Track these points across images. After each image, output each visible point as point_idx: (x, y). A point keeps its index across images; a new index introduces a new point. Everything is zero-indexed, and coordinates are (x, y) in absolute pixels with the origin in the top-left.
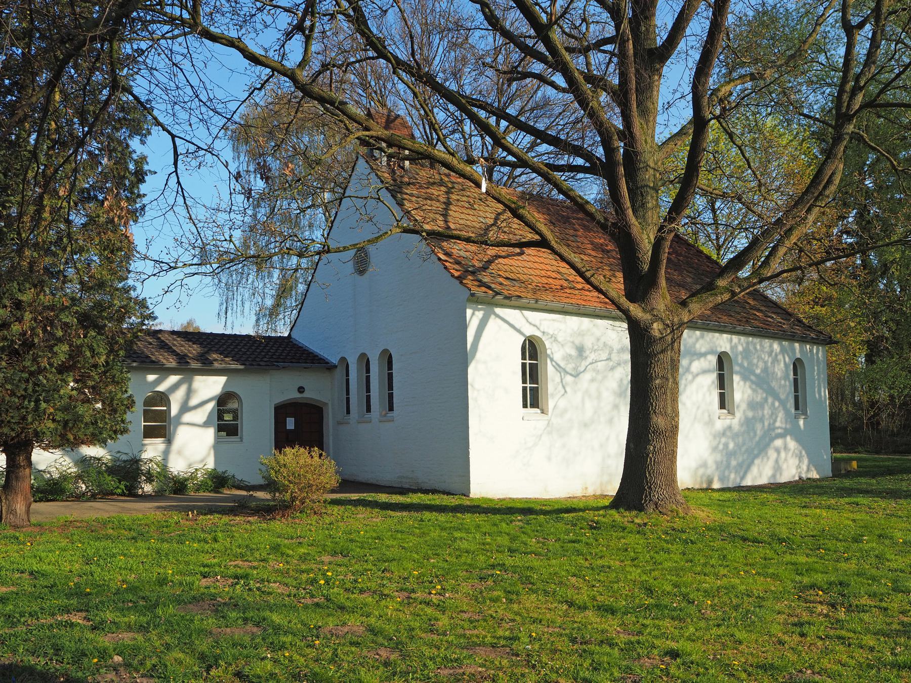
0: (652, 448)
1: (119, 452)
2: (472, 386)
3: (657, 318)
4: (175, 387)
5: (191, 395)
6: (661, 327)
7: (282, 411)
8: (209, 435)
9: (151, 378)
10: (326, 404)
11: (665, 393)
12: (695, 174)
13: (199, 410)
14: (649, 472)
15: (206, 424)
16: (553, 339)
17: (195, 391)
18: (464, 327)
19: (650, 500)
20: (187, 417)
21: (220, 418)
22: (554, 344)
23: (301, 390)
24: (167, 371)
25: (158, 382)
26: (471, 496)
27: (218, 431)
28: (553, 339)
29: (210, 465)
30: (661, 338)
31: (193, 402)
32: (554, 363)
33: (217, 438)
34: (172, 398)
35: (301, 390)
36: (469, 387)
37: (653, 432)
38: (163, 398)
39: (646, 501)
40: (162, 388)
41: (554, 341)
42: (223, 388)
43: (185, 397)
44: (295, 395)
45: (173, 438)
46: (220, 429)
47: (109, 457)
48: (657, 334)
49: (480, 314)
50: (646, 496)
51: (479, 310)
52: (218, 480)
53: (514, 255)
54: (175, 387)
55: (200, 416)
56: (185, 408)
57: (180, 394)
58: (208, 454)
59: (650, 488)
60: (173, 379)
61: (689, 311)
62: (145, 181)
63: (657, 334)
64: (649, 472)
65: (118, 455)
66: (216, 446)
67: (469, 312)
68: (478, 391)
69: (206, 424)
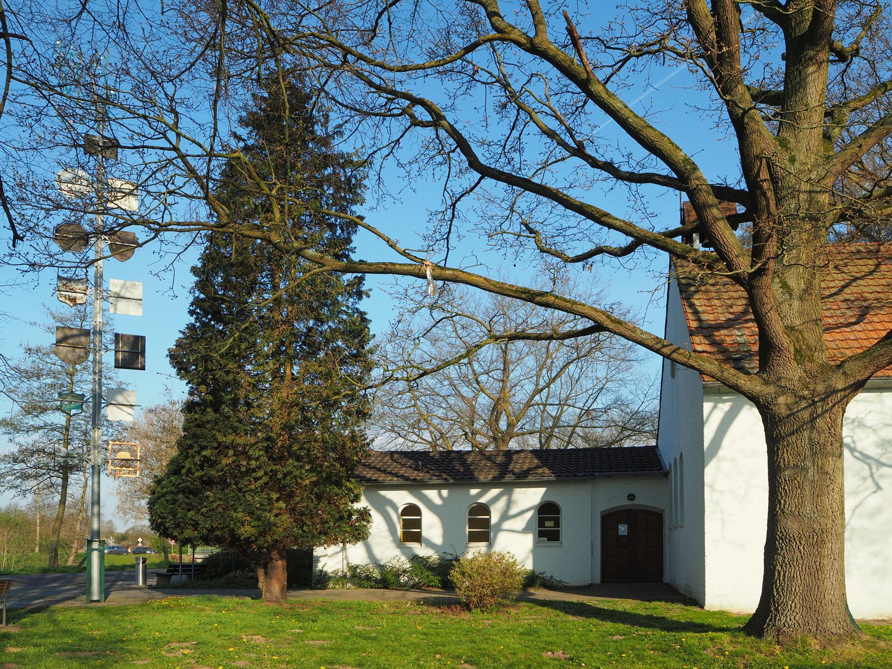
0: (780, 559)
1: (445, 553)
2: (711, 487)
3: (783, 390)
4: (496, 499)
5: (511, 505)
6: (790, 400)
7: (609, 520)
8: (528, 541)
9: (474, 492)
10: (663, 510)
11: (801, 486)
12: (758, 192)
13: (519, 519)
14: (777, 590)
15: (525, 531)
16: (856, 424)
17: (515, 502)
18: (700, 424)
19: (773, 626)
20: (507, 525)
21: (541, 523)
22: (857, 430)
23: (631, 497)
24: (486, 486)
25: (479, 495)
26: (705, 608)
27: (540, 536)
28: (856, 424)
29: (529, 566)
30: (789, 416)
31: (513, 511)
32: (857, 454)
33: (536, 544)
34: (492, 509)
35: (631, 497)
36: (706, 489)
37: (781, 538)
38: (485, 509)
39: (768, 625)
40: (483, 500)
41: (859, 426)
42: (542, 498)
43: (505, 507)
44: (622, 502)
45: (494, 542)
46: (541, 534)
47: (436, 557)
48: (783, 411)
49: (725, 407)
50: (771, 620)
51: (724, 402)
52: (532, 580)
53: (839, 328)
54: (496, 499)
55: (519, 523)
56: (505, 517)
57: (501, 503)
58: (528, 557)
59: (777, 609)
60: (494, 492)
61: (844, 373)
62: (169, 350)
63: (784, 412)
64: (777, 590)
65: (444, 555)
66: (535, 551)
67: (707, 406)
68: (721, 492)
69: (525, 531)
